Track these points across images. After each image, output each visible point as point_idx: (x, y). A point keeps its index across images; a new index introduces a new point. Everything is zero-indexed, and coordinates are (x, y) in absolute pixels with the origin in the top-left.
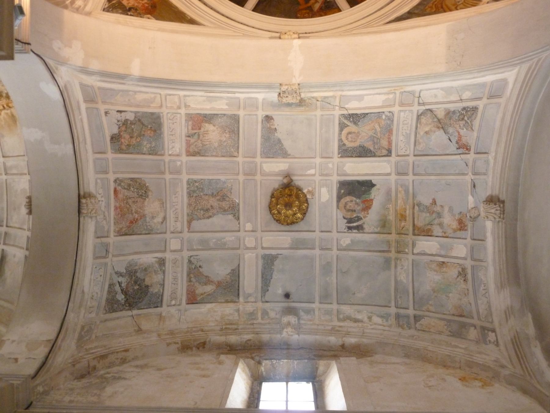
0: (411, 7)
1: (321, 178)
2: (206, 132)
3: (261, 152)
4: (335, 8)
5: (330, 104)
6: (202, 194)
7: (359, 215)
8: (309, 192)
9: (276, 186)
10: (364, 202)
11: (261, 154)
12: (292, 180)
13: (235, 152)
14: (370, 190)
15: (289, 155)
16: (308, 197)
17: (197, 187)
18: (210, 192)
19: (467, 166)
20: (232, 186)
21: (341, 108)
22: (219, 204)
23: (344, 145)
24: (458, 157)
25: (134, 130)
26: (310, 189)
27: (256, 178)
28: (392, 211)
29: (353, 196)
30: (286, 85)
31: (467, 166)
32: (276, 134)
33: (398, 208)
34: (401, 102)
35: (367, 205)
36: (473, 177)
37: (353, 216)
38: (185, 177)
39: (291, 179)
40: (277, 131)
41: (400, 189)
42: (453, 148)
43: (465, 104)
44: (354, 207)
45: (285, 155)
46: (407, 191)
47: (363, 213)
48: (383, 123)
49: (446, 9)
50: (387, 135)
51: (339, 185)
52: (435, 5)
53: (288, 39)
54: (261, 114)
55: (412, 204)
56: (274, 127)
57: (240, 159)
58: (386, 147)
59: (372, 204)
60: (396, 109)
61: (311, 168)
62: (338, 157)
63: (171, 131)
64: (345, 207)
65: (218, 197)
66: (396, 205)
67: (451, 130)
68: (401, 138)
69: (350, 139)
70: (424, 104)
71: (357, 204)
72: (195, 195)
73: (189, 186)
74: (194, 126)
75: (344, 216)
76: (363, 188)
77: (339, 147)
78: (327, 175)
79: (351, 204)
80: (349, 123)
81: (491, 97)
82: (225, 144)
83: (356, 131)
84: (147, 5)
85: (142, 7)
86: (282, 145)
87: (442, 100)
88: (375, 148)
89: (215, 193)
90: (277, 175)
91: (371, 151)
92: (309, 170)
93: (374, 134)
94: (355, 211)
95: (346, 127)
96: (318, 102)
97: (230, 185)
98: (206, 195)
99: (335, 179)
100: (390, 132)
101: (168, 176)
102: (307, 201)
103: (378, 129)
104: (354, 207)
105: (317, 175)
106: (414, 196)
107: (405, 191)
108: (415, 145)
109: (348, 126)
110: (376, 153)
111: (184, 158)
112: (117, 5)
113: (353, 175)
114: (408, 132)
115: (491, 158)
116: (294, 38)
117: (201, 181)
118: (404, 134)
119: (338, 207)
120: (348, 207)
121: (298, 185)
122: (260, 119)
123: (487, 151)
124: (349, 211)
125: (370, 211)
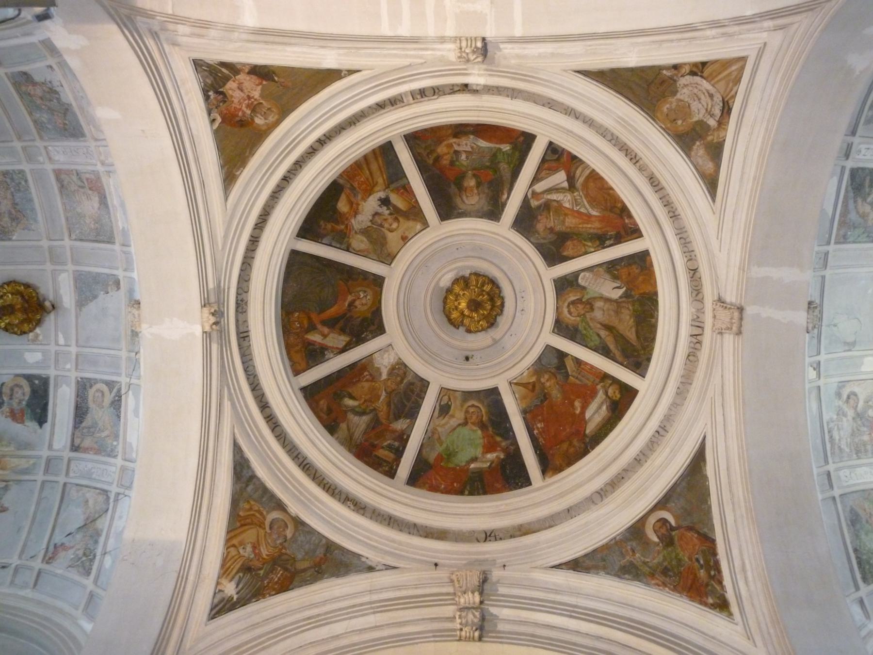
0: (263, 480)
1: (53, 352)
2: (89, 198)
3: (81, 271)
4: (308, 363)
5: (134, 370)
6: (12, 189)
7: (5, 404)
8: (37, 336)
9: (42, 291)
10: (22, 411)
11: (78, 271)
12: (49, 313)
13: (76, 235)
14: (35, 419)
15: (80, 310)
16: (31, 334)
17: (20, 183)
18: (18, 200)
19: (31, 558)
20: (33, 230)
21: (129, 385)
22: (5, 213)
23: (91, 387)
24: (44, 546)
25: (52, 102)
26: (41, 338)
27: (48, 264)
28: (6, 450)
29: (30, 396)
30: (139, 315)
31: (31, 558)
32: (102, 293)
33: (9, 459)
34: (127, 469)
35: (17, 415)
36: (13, 566)
37: (5, 396)
38: (25, 167)
39: (50, 312)
40: (106, 295)
41: (32, 462)
42: (58, 538)
43: (98, 558)
44: (16, 398)
45: (81, 303)
46: (26, 471)
47: (8, 409)
48: (109, 442)
49: (232, 534)
50: (96, 446)
51: (45, 378)
52: (253, 515)
53: (202, 318)
54: (120, 274)
55: (7, 478)
56: (109, 290)
57: (67, 242)
58: (82, 445)
59: (18, 423)
60: (119, 461)
61: (66, 338)
62: (76, 378)
63: (75, 151)
64: (17, 385)
65: (13, 211)
66: (12, 456)
67: (79, 536)
68: (90, 465)
69: (97, 394)
70: (116, 500)
71: (20, 402)
72: (8, 180)
73: (17, 172)
74: (91, 182)
75: (6, 384)
76: (38, 411)
77: (89, 379)
78: (57, 361)
79: (20, 393)
80: (113, 394)
81: (92, 595)
82: (82, 222)
83: (104, 404)
84: (240, 114)
85: (233, 108)
86: (91, 301)
87: (114, 525)
88: (83, 429)
89: (18, 207)
90: (56, 292)
91: (81, 422)
92: (64, 337)
93: (99, 429)
94: (11, 399)
95: (110, 390)
96: (135, 354)
97: (33, 227)
98: (13, 196)
99: (52, 373)
100: (98, 452)
101: (18, 145)
102: (23, 333)
103: (104, 435)
104: (16, 398)
105: (57, 348)
106: (19, 482)
107: (27, 469)
108: (77, 485)
109: (111, 392)
110: (78, 430)
111: (49, 167)
112: (220, 75)
113: (55, 396)
114: (94, 476)
115: (28, 593)
116: (203, 327)
117: (27, 188)
118: (93, 470)
119: (17, 375)
120: (16, 389)
121: (45, 320)
122: (115, 272)
123: (37, 587)
124: (12, 390)
125: (9, 420)
